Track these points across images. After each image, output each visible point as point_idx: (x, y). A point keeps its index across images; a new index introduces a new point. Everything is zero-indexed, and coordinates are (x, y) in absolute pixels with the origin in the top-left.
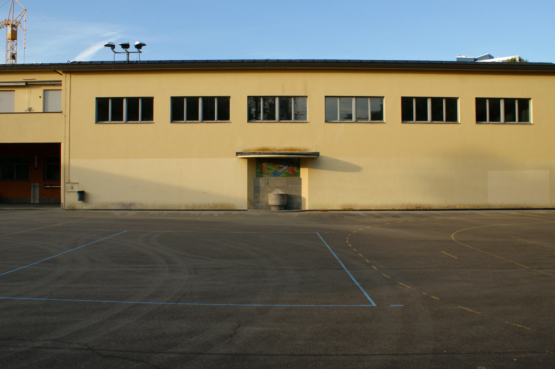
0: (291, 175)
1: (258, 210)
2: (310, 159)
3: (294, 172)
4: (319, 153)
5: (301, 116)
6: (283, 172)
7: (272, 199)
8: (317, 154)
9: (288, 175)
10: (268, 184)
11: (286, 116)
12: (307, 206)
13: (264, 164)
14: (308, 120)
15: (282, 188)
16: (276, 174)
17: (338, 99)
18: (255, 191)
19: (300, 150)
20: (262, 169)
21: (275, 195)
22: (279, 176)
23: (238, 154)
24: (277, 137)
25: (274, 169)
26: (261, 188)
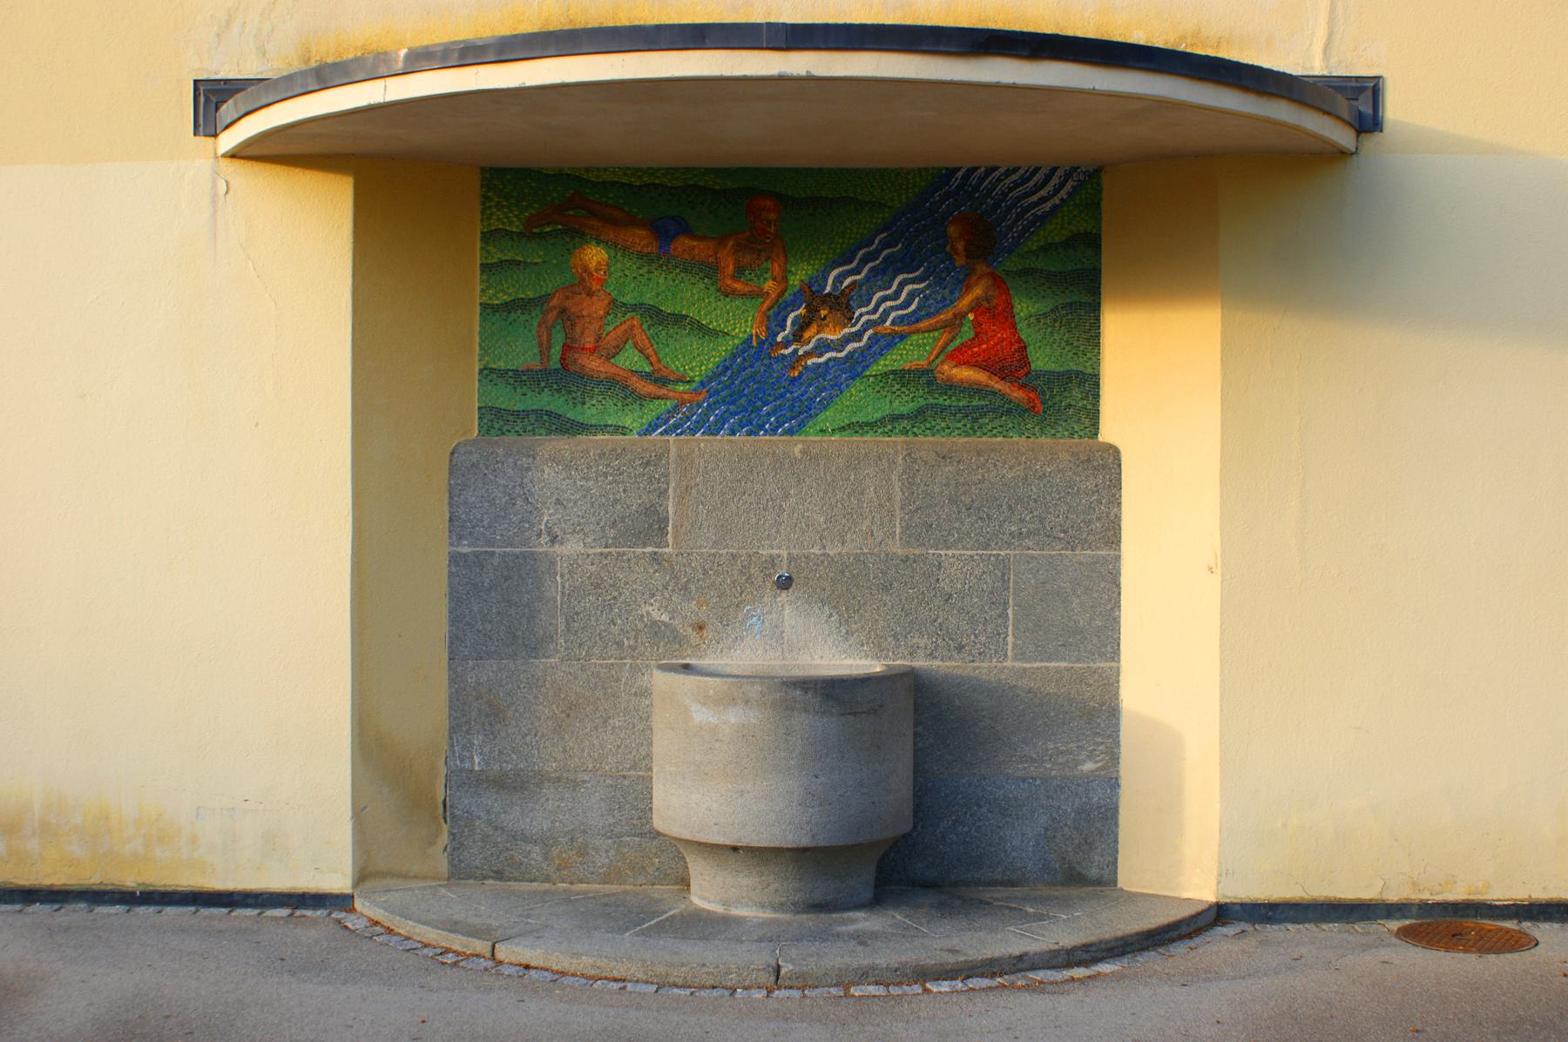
0: (977, 412)
9: (930, 403)
13: (595, 255)
16: (757, 395)
25: (740, 323)
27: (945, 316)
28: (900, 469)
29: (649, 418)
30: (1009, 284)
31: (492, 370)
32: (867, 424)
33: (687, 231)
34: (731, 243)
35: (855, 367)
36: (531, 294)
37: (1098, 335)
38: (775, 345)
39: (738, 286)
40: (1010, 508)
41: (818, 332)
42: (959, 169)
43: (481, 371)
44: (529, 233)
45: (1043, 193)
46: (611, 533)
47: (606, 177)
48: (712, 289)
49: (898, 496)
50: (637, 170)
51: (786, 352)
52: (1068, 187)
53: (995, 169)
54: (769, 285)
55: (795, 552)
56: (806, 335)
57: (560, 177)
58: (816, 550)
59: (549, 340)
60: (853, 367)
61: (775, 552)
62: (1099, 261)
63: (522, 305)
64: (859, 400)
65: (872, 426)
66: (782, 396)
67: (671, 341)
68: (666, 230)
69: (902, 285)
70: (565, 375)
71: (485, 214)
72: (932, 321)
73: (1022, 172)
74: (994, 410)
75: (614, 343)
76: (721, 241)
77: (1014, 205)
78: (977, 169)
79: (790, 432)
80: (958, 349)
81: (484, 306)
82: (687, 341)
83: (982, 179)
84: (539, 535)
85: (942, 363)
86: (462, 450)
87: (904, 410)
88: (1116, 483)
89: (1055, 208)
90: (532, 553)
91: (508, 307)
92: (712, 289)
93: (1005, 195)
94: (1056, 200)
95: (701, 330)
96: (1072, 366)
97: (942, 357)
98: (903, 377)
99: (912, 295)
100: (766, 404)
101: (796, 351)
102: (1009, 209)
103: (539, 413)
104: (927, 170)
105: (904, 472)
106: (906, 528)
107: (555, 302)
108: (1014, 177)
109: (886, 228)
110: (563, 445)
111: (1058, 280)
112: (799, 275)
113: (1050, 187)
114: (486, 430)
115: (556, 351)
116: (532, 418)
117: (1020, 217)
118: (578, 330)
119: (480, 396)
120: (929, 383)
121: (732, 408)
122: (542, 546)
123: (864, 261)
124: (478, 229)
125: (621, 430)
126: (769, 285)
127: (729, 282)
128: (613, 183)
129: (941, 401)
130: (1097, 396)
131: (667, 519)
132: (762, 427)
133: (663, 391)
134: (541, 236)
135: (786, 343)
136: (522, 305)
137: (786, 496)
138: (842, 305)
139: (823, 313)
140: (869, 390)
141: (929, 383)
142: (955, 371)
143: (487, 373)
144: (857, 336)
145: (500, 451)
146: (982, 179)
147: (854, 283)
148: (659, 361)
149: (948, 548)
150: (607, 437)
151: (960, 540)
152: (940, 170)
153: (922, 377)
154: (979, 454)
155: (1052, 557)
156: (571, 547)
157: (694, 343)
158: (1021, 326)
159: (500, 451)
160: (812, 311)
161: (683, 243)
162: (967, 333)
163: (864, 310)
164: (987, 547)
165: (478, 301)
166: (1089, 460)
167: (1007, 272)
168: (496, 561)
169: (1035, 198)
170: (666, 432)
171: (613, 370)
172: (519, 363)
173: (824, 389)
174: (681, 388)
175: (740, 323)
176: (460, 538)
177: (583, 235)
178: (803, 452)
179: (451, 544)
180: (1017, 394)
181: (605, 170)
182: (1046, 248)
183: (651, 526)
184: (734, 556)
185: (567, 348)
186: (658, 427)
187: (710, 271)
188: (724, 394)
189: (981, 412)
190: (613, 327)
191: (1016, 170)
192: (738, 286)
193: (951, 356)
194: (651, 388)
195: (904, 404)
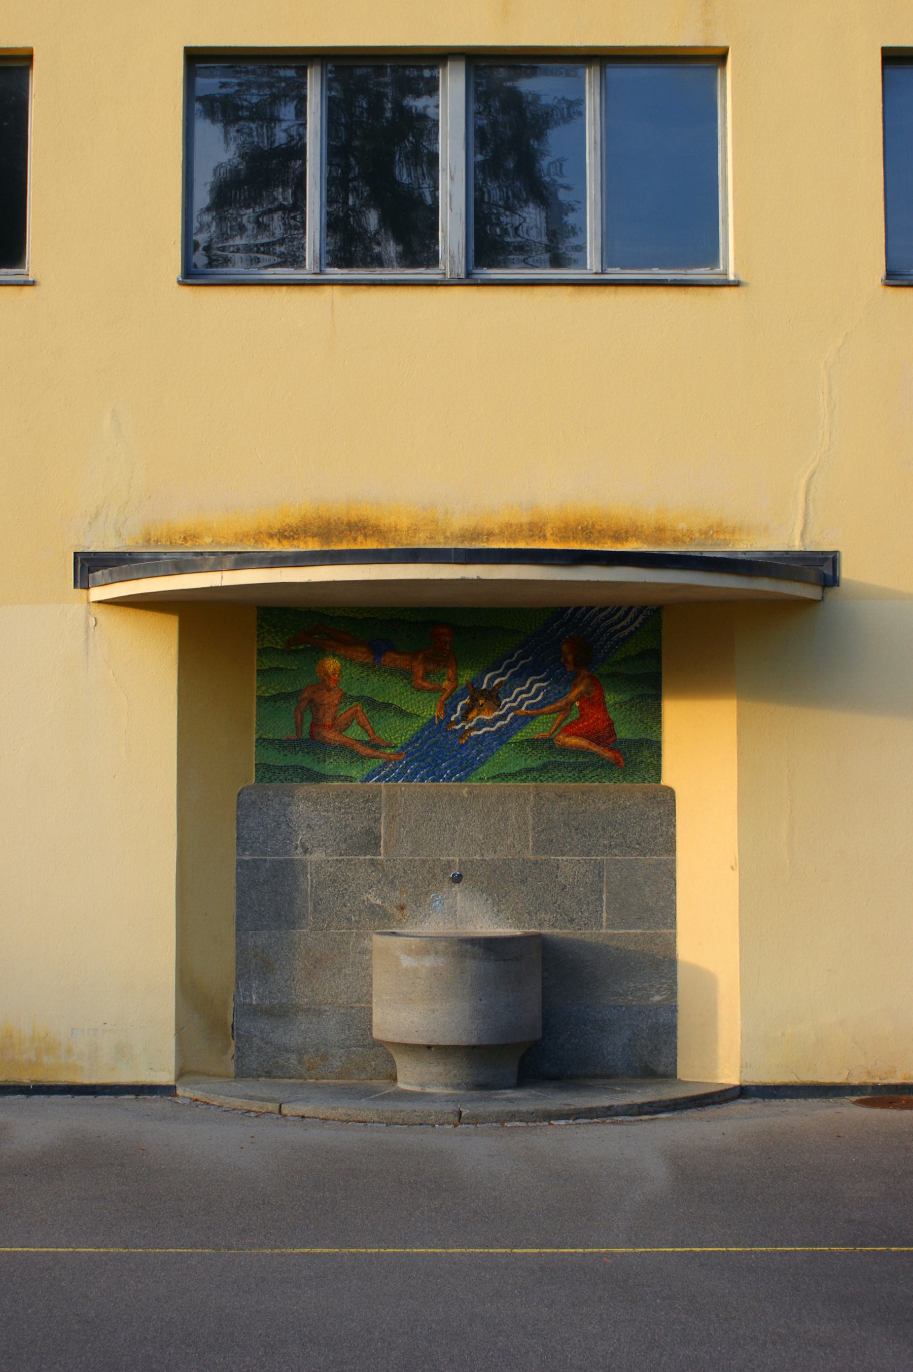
0: (582, 766)
1: (261, 1087)
2: (754, 615)
3: (604, 735)
4: (832, 559)
5: (673, 233)
6: (502, 736)
7: (406, 988)
8: (821, 569)
9: (552, 760)
10: (369, 842)
11: (519, 230)
12: (723, 1046)
13: (332, 664)
14: (731, 263)
15: (495, 882)
16: (439, 755)
17: (591, 78)
18: (253, 922)
19: (660, 532)
20: (314, 706)
21: (430, 945)
22: (465, 769)
23: (89, 566)
24: (456, 416)
25: (428, 709)
26: (307, 883)
27: (561, 703)
28: (532, 804)
31: (265, 740)
32: (510, 774)
35: (502, 736)
36: (290, 689)
40: (603, 829)
42: (569, 608)
43: (257, 740)
45: (624, 623)
46: (343, 846)
49: (531, 821)
51: (457, 727)
52: (641, 617)
54: (446, 684)
58: (478, 857)
64: (505, 758)
66: (455, 756)
69: (532, 684)
70: (313, 743)
72: (552, 707)
73: (610, 610)
75: (345, 722)
80: (569, 725)
81: (259, 698)
82: (392, 720)
83: (584, 615)
84: (296, 848)
85: (559, 734)
87: (534, 765)
89: (631, 634)
90: (292, 860)
92: (409, 686)
94: (632, 628)
96: (643, 736)
97: (558, 731)
98: (534, 744)
101: (463, 727)
103: (295, 768)
105: (535, 806)
112: (466, 677)
113: (628, 619)
114: (260, 779)
115: (306, 727)
119: (257, 756)
120: (550, 748)
122: (298, 855)
126: (446, 684)
127: (420, 682)
129: (558, 759)
131: (380, 837)
132: (441, 777)
133: (377, 753)
135: (457, 722)
137: (458, 822)
139: (481, 702)
140: (511, 752)
141: (550, 748)
142: (567, 740)
143: (261, 741)
144: (503, 717)
146: (584, 615)
147: (501, 682)
148: (374, 733)
150: (340, 783)
151: (571, 850)
155: (631, 860)
156: (317, 856)
159: (271, 793)
162: (575, 714)
163: (508, 700)
164: (588, 854)
166: (654, 797)
168: (268, 865)
169: (618, 627)
171: (344, 739)
175: (428, 709)
176: (244, 850)
178: (469, 793)
179: (238, 854)
180: (608, 755)
181: (339, 609)
183: (370, 841)
184: (424, 861)
185: (314, 725)
186: (373, 777)
187: (407, 675)
188: (416, 755)
190: (344, 712)
191: (606, 608)
193: (565, 730)
194: (369, 751)
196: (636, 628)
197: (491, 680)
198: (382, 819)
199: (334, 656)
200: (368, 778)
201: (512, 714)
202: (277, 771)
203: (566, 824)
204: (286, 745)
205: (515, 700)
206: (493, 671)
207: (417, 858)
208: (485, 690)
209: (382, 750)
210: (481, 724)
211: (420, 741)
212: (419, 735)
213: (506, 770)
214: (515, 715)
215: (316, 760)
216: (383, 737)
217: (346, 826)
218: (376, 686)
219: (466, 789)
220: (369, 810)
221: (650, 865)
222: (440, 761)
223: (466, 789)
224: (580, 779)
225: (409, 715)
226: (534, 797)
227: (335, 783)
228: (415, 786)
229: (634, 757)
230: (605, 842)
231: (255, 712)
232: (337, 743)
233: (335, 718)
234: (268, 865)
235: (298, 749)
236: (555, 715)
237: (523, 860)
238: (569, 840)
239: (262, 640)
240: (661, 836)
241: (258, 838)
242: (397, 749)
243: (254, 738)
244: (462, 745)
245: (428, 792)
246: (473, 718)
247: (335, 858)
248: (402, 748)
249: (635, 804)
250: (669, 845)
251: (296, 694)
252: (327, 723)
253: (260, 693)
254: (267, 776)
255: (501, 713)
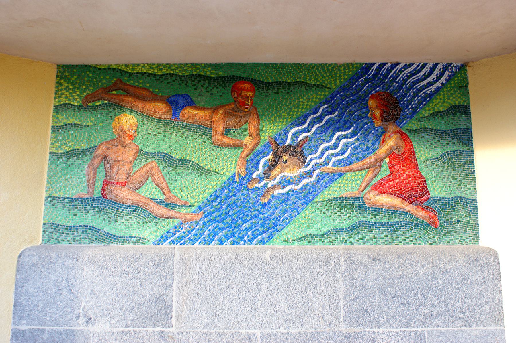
0: (395, 226)
3: (416, 192)
9: (360, 219)
13: (128, 120)
16: (237, 216)
25: (228, 164)
27: (371, 159)
28: (342, 268)
29: (162, 231)
30: (411, 138)
31: (55, 198)
32: (317, 236)
33: (190, 103)
34: (221, 112)
35: (308, 196)
36: (84, 146)
37: (473, 173)
38: (250, 180)
39: (225, 140)
40: (423, 296)
41: (282, 172)
42: (374, 64)
43: (47, 198)
44: (86, 106)
45: (430, 79)
46: (130, 316)
47: (138, 70)
48: (208, 142)
49: (342, 288)
50: (159, 65)
51: (259, 185)
52: (447, 74)
53: (398, 64)
54: (247, 140)
55: (266, 331)
56: (274, 173)
57: (109, 70)
58: (282, 330)
59: (95, 177)
60: (305, 197)
61: (251, 331)
62: (470, 122)
63: (77, 153)
64: (314, 219)
65: (320, 237)
66: (256, 216)
67: (178, 178)
68: (177, 103)
69: (339, 139)
70: (103, 200)
71: (58, 94)
72: (361, 163)
73: (415, 66)
74: (406, 225)
75: (139, 179)
76: (215, 110)
77: (411, 87)
78: (385, 64)
79: (263, 242)
80: (380, 183)
81: (53, 154)
82: (189, 178)
83: (389, 71)
84: (78, 317)
85: (369, 192)
86: (27, 253)
87: (344, 226)
88: (497, 276)
89: (438, 89)
90: (73, 331)
91: (68, 155)
92: (208, 142)
93: (405, 80)
94: (438, 84)
95: (200, 170)
96: (457, 194)
97: (368, 188)
98: (342, 202)
99: (347, 145)
100: (245, 222)
101: (265, 185)
102: (408, 90)
103: (86, 228)
104: (352, 64)
105: (346, 271)
106: (349, 312)
107: (99, 152)
108: (410, 69)
109: (326, 102)
110: (98, 250)
111: (441, 135)
112: (269, 130)
113: (434, 76)
114: (47, 240)
115: (99, 185)
116: (80, 231)
117: (416, 95)
118: (115, 170)
119: (45, 215)
120: (360, 207)
121: (221, 225)
122: (80, 326)
123: (313, 123)
124: (53, 103)
125: (141, 240)
126: (247, 140)
127: (219, 137)
128: (143, 74)
129: (369, 219)
130: (476, 214)
131: (171, 306)
132: (242, 238)
133: (172, 213)
134: (93, 108)
135: (260, 179)
136: (77, 153)
137: (260, 289)
138: (297, 152)
139: (285, 158)
140: (318, 212)
141: (360, 207)
142: (378, 198)
143: (51, 199)
144: (309, 174)
145: (53, 255)
146: (389, 71)
147: (306, 137)
148: (170, 191)
149: (379, 327)
150: (132, 245)
151: (388, 320)
152: (361, 64)
153: (356, 202)
154: (399, 257)
155: (455, 332)
156: (101, 327)
157: (190, 177)
158: (421, 166)
159: (53, 255)
160: (277, 157)
161: (189, 111)
162: (385, 171)
163: (313, 156)
164: (408, 325)
165: (48, 151)
166: (477, 260)
167: (411, 131)
168: (46, 336)
169: (425, 83)
170: (173, 242)
171: (138, 198)
172: (73, 193)
173: (285, 211)
174: (184, 210)
175: (228, 164)
176: (21, 318)
177: (121, 107)
178: (273, 257)
179: (14, 323)
180: (421, 214)
181: (138, 65)
182: (434, 115)
183: (159, 311)
184: (220, 335)
185: (106, 183)
186: (167, 238)
187: (207, 129)
188: (214, 215)
189: (397, 226)
190: (139, 168)
191: (411, 65)
192: (225, 140)
193: (375, 188)
194: (162, 211)
195: (343, 222)
196: (442, 84)
197: (295, 136)
198: (175, 285)
199: (131, 111)
200: (163, 239)
201: (317, 172)
202: (65, 231)
203: (382, 292)
204: (76, 203)
205: (321, 157)
206: (297, 125)
207: (213, 331)
208: (289, 146)
209: (177, 210)
210: (283, 184)
211: (219, 200)
212: (218, 194)
213: (313, 231)
214: (322, 172)
215: (107, 220)
216: (179, 196)
217: (134, 293)
218: (174, 141)
219: (269, 252)
220: (160, 276)
221: (476, 336)
222: (240, 222)
223: (269, 252)
224: (394, 240)
225: (208, 172)
226: (345, 261)
227: (126, 245)
228: (212, 248)
229: (449, 216)
230: (426, 311)
231: (47, 170)
232: (130, 202)
233: (129, 176)
234: (46, 336)
235: (88, 208)
236: (364, 172)
237: (335, 333)
238: (385, 309)
239: (60, 97)
240: (487, 303)
241: (37, 306)
242: (194, 209)
243: (44, 195)
244: (264, 205)
245: (227, 255)
246: (276, 176)
247: (121, 329)
248: (200, 208)
249: (457, 268)
250: (495, 314)
251: (91, 150)
252: (120, 181)
253: (54, 150)
254: (55, 237)
255: (306, 170)
